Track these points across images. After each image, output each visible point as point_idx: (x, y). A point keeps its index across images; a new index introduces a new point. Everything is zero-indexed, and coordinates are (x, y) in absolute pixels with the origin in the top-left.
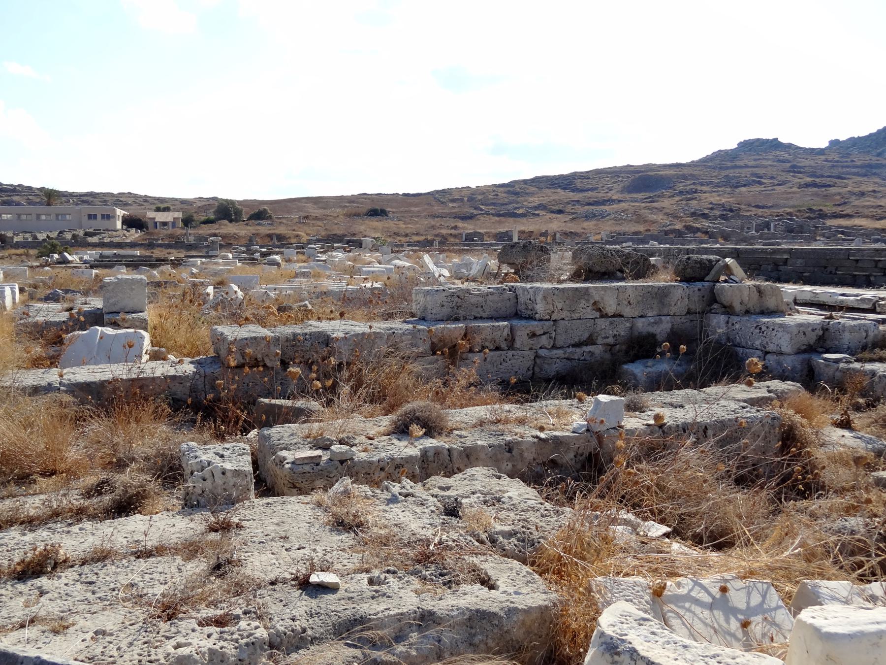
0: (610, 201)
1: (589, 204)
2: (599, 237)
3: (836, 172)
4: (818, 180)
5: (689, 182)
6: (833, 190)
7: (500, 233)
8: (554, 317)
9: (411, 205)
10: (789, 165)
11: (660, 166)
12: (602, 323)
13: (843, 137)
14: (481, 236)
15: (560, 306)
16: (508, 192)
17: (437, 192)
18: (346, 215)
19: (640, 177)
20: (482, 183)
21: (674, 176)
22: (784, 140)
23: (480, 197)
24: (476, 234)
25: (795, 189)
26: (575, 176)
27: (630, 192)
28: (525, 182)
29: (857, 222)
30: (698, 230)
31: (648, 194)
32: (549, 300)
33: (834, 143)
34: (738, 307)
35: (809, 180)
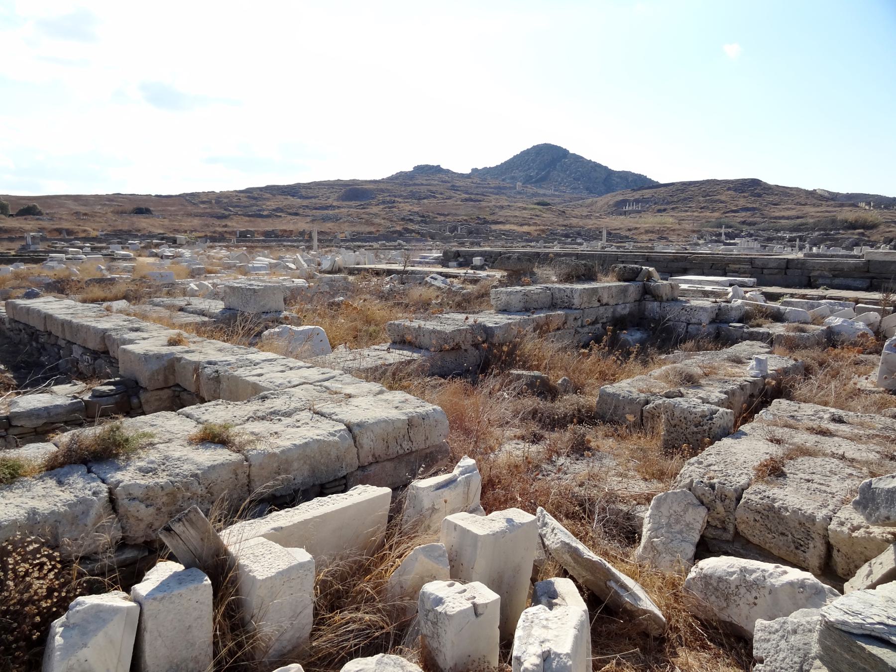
0: (331, 207)
1: (316, 209)
2: (343, 235)
3: (480, 190)
4: (473, 197)
5: (386, 194)
6: (484, 204)
7: (268, 231)
9: (167, 205)
10: (449, 185)
11: (366, 181)
12: (602, 309)
13: (480, 167)
14: (252, 233)
16: (249, 197)
17: (187, 195)
18: (112, 212)
19: (350, 190)
20: (225, 189)
21: (374, 190)
22: (444, 167)
23: (226, 200)
24: (248, 232)
25: (459, 202)
26: (298, 186)
27: (343, 200)
28: (261, 189)
29: (507, 227)
30: (413, 231)
31: (359, 203)
33: (475, 170)
34: (665, 298)
35: (467, 196)
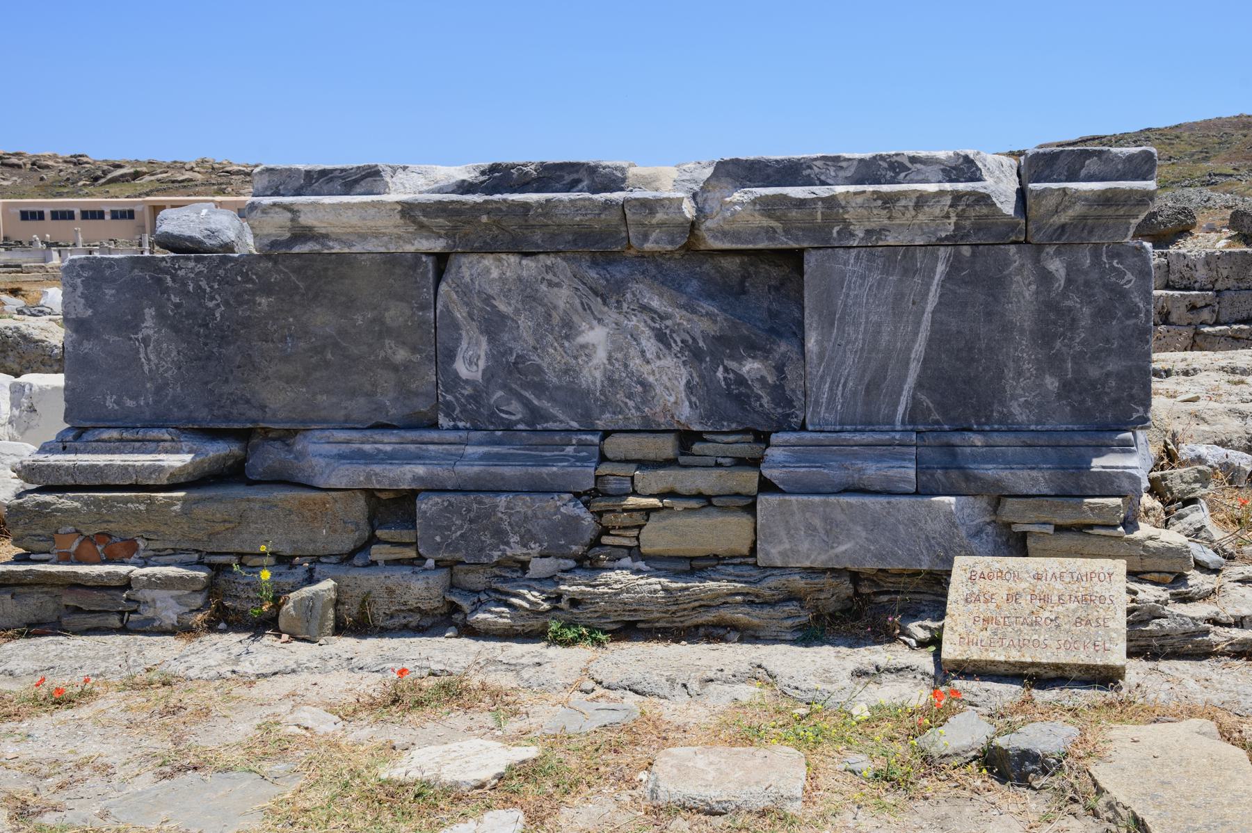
8: (1218, 286)
15: (1225, 273)
22: (727, 158)
32: (1213, 266)
